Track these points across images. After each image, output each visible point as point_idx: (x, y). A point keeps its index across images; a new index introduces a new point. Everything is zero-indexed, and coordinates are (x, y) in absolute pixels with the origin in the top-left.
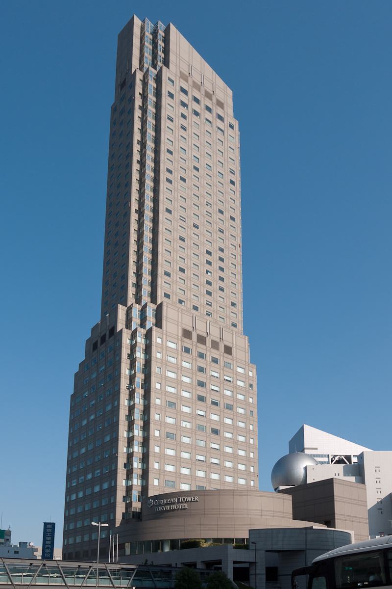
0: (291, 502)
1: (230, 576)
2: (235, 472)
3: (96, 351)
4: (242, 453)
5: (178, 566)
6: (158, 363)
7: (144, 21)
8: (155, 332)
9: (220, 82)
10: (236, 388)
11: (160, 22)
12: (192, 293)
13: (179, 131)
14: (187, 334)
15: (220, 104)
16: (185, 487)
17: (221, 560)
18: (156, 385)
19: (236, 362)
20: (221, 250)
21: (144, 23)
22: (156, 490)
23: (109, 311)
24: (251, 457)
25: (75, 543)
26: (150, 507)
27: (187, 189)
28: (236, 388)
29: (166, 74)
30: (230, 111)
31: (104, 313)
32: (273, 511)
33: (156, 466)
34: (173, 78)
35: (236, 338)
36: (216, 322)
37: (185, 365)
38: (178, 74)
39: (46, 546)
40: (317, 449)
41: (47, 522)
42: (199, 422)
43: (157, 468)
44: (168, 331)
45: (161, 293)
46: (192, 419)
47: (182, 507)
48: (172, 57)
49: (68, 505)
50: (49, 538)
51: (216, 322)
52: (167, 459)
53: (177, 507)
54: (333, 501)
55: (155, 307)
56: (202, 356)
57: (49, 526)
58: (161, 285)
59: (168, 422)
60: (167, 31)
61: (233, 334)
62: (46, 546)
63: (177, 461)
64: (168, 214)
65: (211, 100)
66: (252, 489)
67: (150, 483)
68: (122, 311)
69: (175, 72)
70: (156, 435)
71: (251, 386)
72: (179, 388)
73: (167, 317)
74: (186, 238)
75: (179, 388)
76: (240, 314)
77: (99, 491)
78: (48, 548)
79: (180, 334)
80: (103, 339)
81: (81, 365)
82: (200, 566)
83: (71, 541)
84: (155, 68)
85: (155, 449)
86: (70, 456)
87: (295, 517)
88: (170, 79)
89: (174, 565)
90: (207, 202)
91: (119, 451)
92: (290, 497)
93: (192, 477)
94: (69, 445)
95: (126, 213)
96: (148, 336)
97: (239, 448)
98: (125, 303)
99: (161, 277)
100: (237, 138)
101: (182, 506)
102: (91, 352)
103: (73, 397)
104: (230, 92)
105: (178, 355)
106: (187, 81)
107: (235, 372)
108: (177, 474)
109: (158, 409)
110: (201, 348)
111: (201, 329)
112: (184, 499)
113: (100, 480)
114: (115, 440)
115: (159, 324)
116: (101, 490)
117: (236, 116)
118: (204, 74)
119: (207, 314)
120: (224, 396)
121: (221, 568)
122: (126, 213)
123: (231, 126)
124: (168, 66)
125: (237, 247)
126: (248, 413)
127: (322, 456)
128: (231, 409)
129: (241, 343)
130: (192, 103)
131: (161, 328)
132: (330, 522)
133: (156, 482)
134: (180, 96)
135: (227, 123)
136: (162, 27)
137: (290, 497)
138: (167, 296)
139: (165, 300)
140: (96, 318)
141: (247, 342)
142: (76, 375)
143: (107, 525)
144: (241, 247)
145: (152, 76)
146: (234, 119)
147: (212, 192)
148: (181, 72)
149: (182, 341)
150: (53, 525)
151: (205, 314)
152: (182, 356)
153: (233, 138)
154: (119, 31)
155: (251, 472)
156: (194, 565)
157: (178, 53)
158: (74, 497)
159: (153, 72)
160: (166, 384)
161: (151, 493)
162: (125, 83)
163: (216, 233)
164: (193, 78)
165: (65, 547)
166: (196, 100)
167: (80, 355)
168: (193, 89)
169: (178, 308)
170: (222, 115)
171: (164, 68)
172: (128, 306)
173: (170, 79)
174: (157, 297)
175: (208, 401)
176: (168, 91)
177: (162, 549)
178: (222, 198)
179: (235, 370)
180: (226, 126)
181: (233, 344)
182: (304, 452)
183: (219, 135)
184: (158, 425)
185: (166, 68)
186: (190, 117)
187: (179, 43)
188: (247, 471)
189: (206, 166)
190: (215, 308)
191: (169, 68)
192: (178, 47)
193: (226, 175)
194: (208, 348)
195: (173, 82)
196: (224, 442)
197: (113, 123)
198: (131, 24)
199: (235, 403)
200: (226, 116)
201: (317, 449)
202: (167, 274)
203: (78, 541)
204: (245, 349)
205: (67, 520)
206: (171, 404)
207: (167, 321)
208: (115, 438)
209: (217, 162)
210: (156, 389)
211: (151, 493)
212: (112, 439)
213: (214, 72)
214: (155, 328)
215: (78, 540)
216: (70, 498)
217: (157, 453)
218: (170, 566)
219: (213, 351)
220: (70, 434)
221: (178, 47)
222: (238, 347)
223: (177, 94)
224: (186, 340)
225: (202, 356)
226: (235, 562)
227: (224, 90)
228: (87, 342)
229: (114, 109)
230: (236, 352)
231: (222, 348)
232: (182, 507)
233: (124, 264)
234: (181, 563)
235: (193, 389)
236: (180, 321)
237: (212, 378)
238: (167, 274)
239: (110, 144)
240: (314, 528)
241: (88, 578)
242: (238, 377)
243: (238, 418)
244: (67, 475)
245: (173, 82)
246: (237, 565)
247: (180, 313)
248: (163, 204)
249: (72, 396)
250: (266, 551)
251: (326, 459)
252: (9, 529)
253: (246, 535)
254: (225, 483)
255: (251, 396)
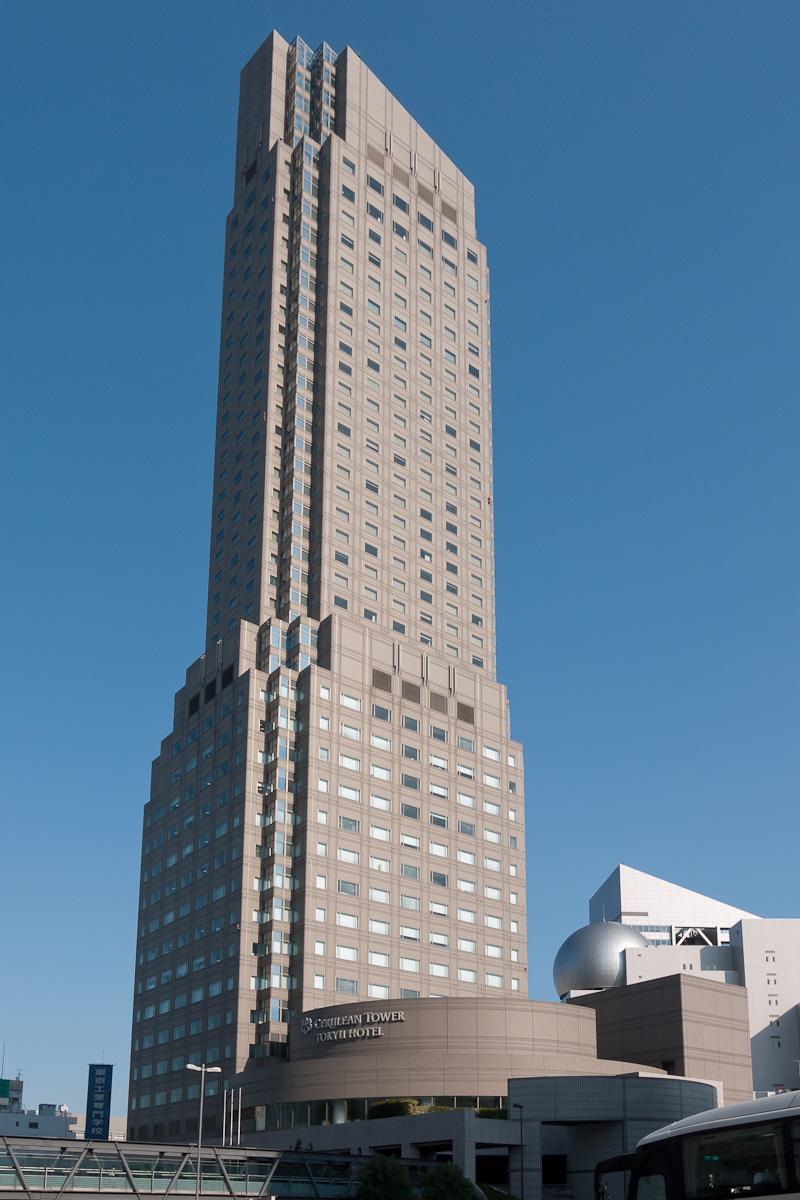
0: (594, 1024)
1: (470, 1174)
2: (479, 962)
3: (196, 715)
4: (493, 923)
5: (364, 1153)
6: (322, 740)
7: (293, 43)
8: (317, 675)
9: (449, 168)
10: (482, 790)
11: (326, 45)
12: (392, 597)
13: (365, 266)
14: (381, 680)
15: (449, 212)
16: (378, 993)
17: (451, 1141)
18: (318, 785)
19: (482, 737)
20: (452, 509)
21: (295, 46)
22: (318, 999)
23: (222, 634)
24: (512, 930)
25: (153, 1107)
26: (305, 1032)
27: (381, 385)
28: (482, 790)
29: (339, 151)
30: (470, 227)
31: (211, 639)
32: (558, 1042)
33: (319, 949)
34: (353, 160)
35: (481, 688)
36: (441, 656)
37: (378, 743)
38: (364, 151)
39: (95, 1112)
40: (646, 914)
41: (96, 1063)
42: (405, 861)
43: (321, 953)
44: (343, 673)
45: (329, 597)
46: (393, 853)
47: (371, 1033)
48: (351, 116)
49: (139, 1029)
50: (100, 1097)
51: (441, 656)
52: (341, 935)
53: (361, 1033)
54: (679, 1021)
55: (316, 625)
56: (411, 725)
57: (100, 1072)
58: (329, 580)
59: (343, 860)
60: (341, 64)
61: (475, 681)
62: (95, 1112)
63: (362, 939)
64: (342, 436)
65: (431, 203)
66: (515, 996)
67: (305, 984)
68: (248, 633)
69: (356, 147)
70: (318, 886)
71: (512, 786)
72: (366, 790)
73: (340, 645)
74: (380, 485)
75: (366, 790)
76: (489, 640)
77: (203, 1001)
78: (98, 1116)
79: (368, 680)
80: (210, 692)
81: (166, 743)
82: (408, 1153)
83: (145, 1102)
84: (316, 138)
85: (315, 915)
86: (143, 929)
87: (603, 1054)
88: (346, 161)
89: (354, 1151)
90: (422, 412)
91: (243, 919)
92: (591, 1013)
93: (393, 972)
94: (140, 906)
95: (258, 433)
96: (303, 684)
97: (488, 913)
98: (254, 618)
99: (329, 565)
100: (484, 282)
101: (371, 1031)
102: (187, 717)
103: (149, 809)
104: (470, 188)
105: (363, 722)
106: (382, 165)
107: (479, 757)
108: (362, 965)
109: (323, 833)
110: (411, 710)
111: (410, 670)
112: (376, 1017)
113: (205, 978)
114: (235, 897)
115: (324, 659)
116: (207, 999)
117: (481, 237)
118: (416, 152)
119: (423, 640)
120: (457, 807)
121: (450, 1158)
122: (258, 433)
123: (472, 258)
124: (342, 135)
125: (484, 503)
126: (507, 841)
127: (657, 929)
128: (471, 833)
129: (491, 699)
130: (392, 210)
131: (329, 669)
132: (673, 1064)
133: (318, 983)
134: (368, 195)
135: (462, 251)
136: (330, 55)
137: (591, 1013)
138: (341, 603)
139: (338, 611)
140: (196, 648)
141: (504, 696)
142: (155, 764)
143: (219, 1070)
144: (492, 503)
145: (310, 156)
146: (477, 242)
147: (432, 391)
148: (369, 146)
149: (371, 694)
150: (109, 1069)
151: (419, 639)
152: (370, 725)
153: (476, 281)
154: (243, 64)
155: (512, 962)
156: (396, 1151)
157: (363, 108)
158: (150, 1013)
159: (313, 147)
160: (338, 782)
161: (309, 1005)
162: (255, 169)
163: (441, 474)
164: (394, 160)
165: (133, 1115)
166: (401, 204)
167: (164, 724)
168: (394, 181)
169: (364, 627)
170: (453, 234)
171: (335, 138)
172: (262, 623)
173: (346, 161)
174: (320, 604)
175: (425, 816)
176: (344, 186)
177: (331, 1119)
178: (454, 403)
179: (479, 753)
180: (461, 257)
181: (475, 700)
182: (621, 921)
183: (448, 275)
184: (322, 866)
185: (338, 138)
186: (388, 238)
187: (365, 87)
188: (505, 960)
189: (420, 338)
190: (439, 627)
191: (344, 139)
192: (363, 96)
193: (462, 356)
194: (424, 709)
195: (352, 166)
196: (457, 900)
197: (231, 251)
198: (267, 49)
199: (480, 822)
200: (461, 237)
201: (646, 914)
202: (342, 559)
203: (159, 1102)
204: (501, 710)
205: (137, 1059)
206: (349, 824)
207: (340, 654)
208: (235, 891)
209: (444, 329)
210: (319, 792)
211: (309, 1005)
212: (228, 894)
213: (436, 146)
214: (315, 668)
215: (160, 1100)
216: (143, 1015)
217: (320, 922)
218: (346, 1153)
219: (436, 714)
220: (142, 884)
221: (363, 96)
222: (485, 707)
223: (362, 192)
224: (379, 692)
225: (411, 725)
226: (479, 1146)
227: (457, 184)
228: (178, 696)
229: (233, 222)
230: (482, 718)
231: (453, 710)
232: (371, 1033)
233: (253, 538)
234: (370, 1148)
235: (393, 792)
236: (367, 654)
237: (432, 770)
238: (342, 559)
239: (224, 293)
240: (640, 1075)
241: (179, 1178)
242: (486, 769)
243: (486, 851)
244: (137, 968)
245: (352, 166)
246: (484, 1152)
247: (367, 639)
248: (334, 416)
249: (147, 807)
250: (544, 1123)
251: (665, 936)
252: (18, 1078)
253: (502, 1091)
254: (458, 983)
255: (513, 806)
